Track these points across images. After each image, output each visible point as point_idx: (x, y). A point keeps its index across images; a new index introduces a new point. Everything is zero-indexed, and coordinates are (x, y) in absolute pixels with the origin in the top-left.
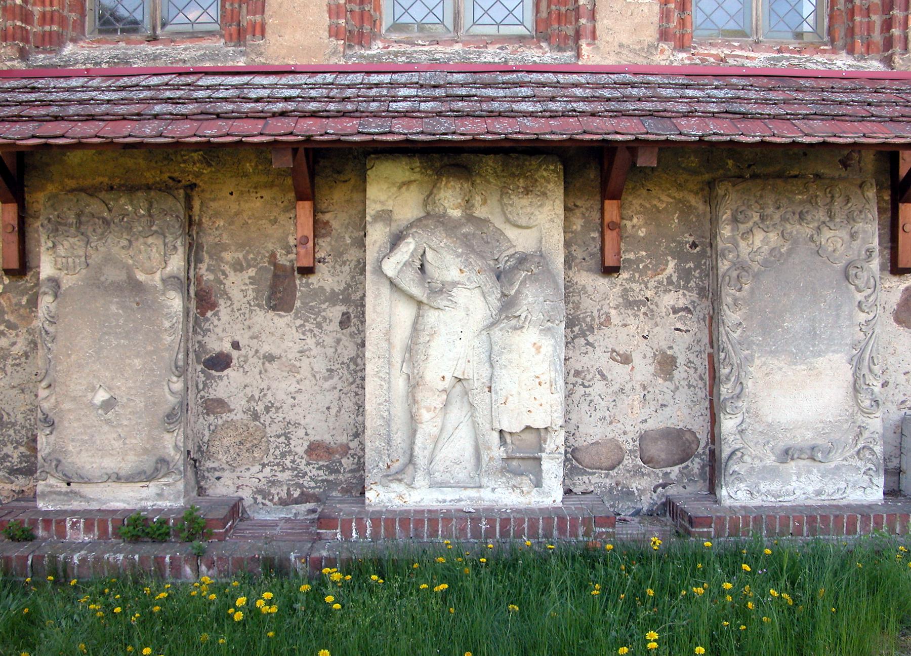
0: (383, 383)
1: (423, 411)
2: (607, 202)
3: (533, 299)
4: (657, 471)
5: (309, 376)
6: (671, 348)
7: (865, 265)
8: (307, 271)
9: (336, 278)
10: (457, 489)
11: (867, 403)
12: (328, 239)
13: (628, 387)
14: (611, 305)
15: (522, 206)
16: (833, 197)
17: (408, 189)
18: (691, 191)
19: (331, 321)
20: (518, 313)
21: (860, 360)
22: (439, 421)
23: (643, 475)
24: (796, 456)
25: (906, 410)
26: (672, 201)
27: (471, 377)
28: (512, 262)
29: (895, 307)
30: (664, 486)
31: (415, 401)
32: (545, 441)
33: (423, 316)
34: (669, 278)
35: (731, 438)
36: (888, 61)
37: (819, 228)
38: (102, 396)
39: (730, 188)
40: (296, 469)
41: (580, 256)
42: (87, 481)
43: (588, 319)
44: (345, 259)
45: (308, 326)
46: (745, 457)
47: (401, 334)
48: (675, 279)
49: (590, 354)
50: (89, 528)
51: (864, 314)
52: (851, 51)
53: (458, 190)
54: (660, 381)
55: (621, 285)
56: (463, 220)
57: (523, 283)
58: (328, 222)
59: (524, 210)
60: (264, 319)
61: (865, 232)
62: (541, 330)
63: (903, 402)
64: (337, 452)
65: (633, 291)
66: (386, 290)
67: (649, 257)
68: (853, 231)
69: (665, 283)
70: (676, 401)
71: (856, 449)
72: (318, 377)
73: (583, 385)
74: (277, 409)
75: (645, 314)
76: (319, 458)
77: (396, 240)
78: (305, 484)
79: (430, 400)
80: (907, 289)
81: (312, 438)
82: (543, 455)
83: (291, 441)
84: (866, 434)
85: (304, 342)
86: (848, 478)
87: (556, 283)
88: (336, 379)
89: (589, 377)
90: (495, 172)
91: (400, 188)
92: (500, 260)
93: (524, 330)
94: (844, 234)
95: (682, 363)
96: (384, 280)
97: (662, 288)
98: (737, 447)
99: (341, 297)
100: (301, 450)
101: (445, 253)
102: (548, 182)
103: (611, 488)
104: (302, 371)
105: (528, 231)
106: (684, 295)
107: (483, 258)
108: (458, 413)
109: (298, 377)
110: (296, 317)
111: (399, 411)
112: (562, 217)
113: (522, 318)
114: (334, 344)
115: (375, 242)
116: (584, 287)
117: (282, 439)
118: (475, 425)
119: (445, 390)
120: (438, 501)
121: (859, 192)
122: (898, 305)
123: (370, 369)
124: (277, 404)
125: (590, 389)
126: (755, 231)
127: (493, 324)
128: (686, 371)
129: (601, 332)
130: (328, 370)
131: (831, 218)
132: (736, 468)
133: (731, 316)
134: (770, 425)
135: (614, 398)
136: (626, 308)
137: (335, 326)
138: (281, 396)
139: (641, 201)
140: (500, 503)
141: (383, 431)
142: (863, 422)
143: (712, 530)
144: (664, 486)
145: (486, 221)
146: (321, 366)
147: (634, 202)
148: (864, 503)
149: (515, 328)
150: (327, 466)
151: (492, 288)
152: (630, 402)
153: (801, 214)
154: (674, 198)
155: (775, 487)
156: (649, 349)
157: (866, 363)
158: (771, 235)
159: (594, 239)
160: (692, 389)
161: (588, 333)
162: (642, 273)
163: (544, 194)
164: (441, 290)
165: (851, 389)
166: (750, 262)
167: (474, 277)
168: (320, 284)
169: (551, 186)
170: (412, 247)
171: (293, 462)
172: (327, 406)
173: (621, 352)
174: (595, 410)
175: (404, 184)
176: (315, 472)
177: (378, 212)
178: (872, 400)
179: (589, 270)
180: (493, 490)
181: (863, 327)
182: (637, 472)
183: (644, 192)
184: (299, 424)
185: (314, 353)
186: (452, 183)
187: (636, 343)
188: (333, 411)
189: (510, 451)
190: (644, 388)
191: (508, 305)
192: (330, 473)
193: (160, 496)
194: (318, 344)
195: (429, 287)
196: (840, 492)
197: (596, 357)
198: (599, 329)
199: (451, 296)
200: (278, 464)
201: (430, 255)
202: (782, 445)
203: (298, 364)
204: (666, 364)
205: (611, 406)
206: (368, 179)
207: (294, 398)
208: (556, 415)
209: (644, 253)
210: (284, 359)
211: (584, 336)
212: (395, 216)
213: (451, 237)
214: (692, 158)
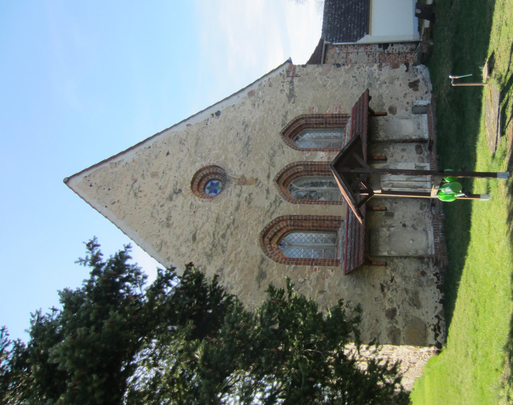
2: (376, 158)
36: (349, 117)
38: (411, 242)
42: (428, 244)
50: (436, 238)
52: (346, 124)
60: (395, 217)
133: (394, 138)
155: (425, 130)
182: (424, 155)
193: (430, 230)
204: (403, 150)
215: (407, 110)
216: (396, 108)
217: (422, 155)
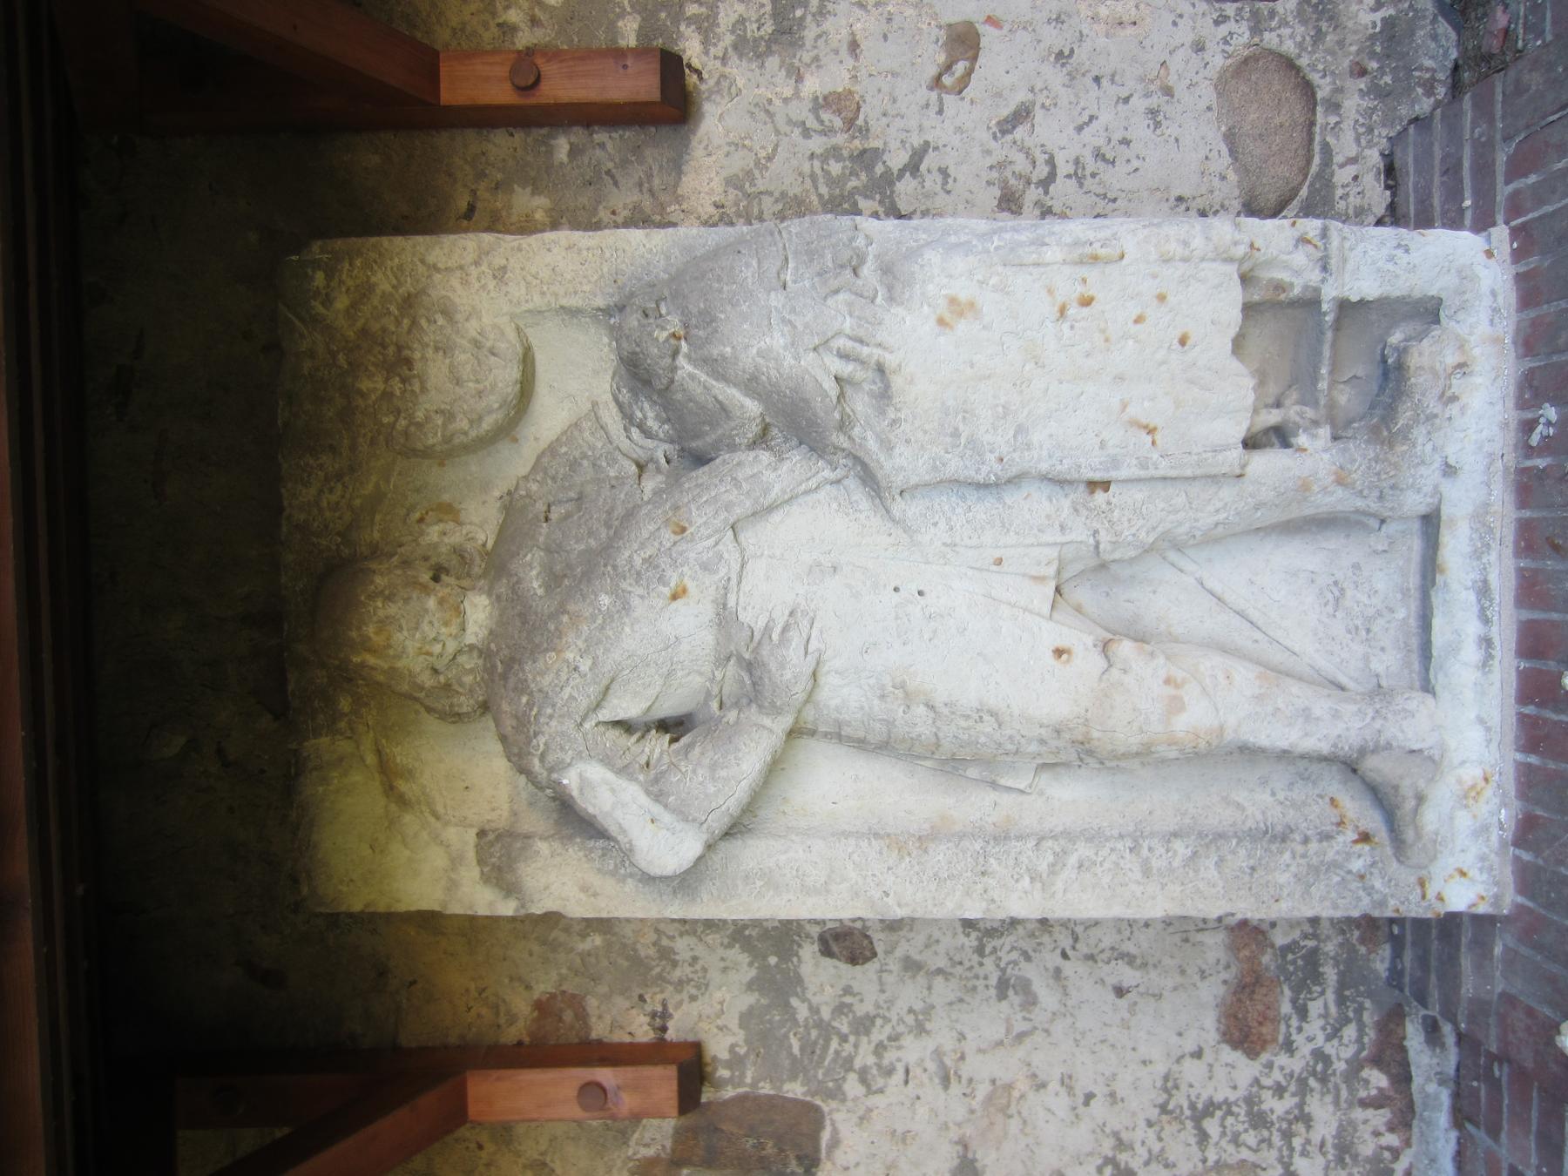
0: (1072, 860)
1: (1182, 724)
2: (447, 96)
3: (776, 330)
5: (1020, 1052)
8: (692, 1069)
9: (714, 975)
10: (1437, 599)
12: (592, 1003)
14: (788, 92)
15: (456, 379)
17: (409, 774)
19: (848, 991)
20: (830, 386)
22: (1211, 664)
27: (1053, 553)
28: (648, 413)
31: (1144, 754)
32: (1279, 287)
33: (839, 724)
40: (1303, 1083)
41: (633, 197)
43: (835, 168)
44: (652, 951)
45: (865, 1057)
47: (900, 794)
49: (949, 161)
53: (393, 609)
55: (724, 60)
56: (502, 588)
57: (717, 368)
58: (539, 1006)
59: (466, 372)
62: (891, 299)
64: (1252, 960)
65: (742, 21)
66: (752, 853)
72: (1025, 1026)
73: (1046, 183)
74: (1121, 1145)
76: (1269, 1017)
77: (572, 820)
78: (1348, 1053)
79: (1142, 701)
81: (1211, 1036)
82: (1330, 293)
83: (1219, 1098)
85: (916, 1071)
87: (715, 254)
88: (1029, 971)
89: (1021, 163)
90: (339, 476)
91: (403, 802)
92: (641, 455)
93: (890, 360)
96: (716, 859)
99: (773, 960)
100: (1245, 1069)
101: (616, 655)
102: (366, 290)
103: (1378, 92)
104: (1004, 1077)
105: (540, 358)
107: (630, 514)
108: (1169, 598)
109: (1022, 1085)
110: (837, 1094)
111: (1162, 802)
112: (487, 238)
113: (846, 369)
114: (921, 979)
115: (584, 889)
116: (732, 182)
117: (1212, 1126)
118: (1215, 538)
119: (1105, 647)
120: (1485, 664)
123: (1023, 903)
124: (1107, 1147)
127: (868, 477)
129: (875, 127)
130: (1002, 996)
135: (1088, 80)
136: (797, 43)
137: (863, 977)
138: (1081, 1137)
140: (1497, 447)
141: (1240, 859)
145: (512, 506)
146: (989, 1019)
147: (454, 21)
149: (884, 395)
150: (1297, 990)
151: (737, 484)
159: (574, 152)
161: (879, 169)
163: (409, 302)
164: (749, 666)
167: (699, 549)
168: (734, 1024)
169: (383, 282)
170: (596, 772)
171: (1279, 1091)
172: (1112, 996)
173: (942, 58)
174: (1126, 142)
175: (390, 789)
176: (1315, 1027)
177: (485, 879)
179: (677, 166)
180: (1449, 470)
184: (1166, 1078)
185: (946, 1040)
186: (370, 630)
188: (1128, 976)
189: (1310, 413)
191: (796, 424)
192: (1317, 977)
194: (920, 1030)
195: (737, 704)
197: (956, 140)
198: (865, 131)
199: (768, 629)
200: (1287, 1135)
201: (628, 706)
203: (983, 1090)
205: (1112, 91)
206: (381, 909)
207: (1089, 1097)
208: (1198, 242)
210: (968, 1131)
211: (889, 180)
212: (499, 816)
213: (560, 634)
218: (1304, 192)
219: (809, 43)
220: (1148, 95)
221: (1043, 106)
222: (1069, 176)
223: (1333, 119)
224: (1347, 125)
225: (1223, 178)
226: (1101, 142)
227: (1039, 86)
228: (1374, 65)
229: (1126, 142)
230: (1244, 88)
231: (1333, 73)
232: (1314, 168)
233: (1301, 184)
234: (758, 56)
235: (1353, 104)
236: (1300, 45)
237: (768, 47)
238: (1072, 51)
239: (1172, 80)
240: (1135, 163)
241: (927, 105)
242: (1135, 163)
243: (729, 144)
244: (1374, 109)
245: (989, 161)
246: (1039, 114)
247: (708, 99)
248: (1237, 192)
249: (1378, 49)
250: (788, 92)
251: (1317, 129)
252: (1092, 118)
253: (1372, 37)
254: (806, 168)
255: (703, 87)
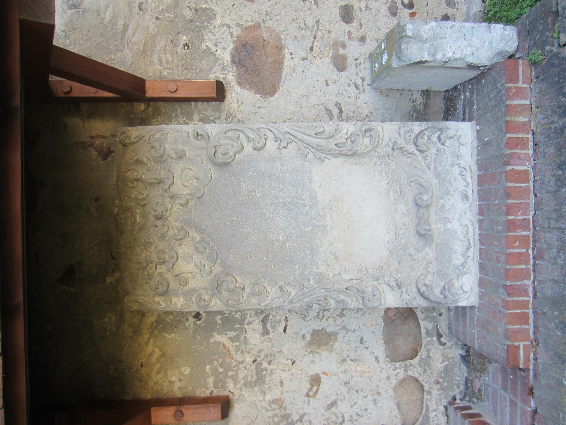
4: (424, 342)
6: (304, 336)
7: (213, 142)
11: (367, 141)
13: (343, 377)
14: (261, 399)
16: (137, 180)
18: (141, 320)
21: (319, 149)
23: (429, 357)
24: (428, 228)
25: (365, 83)
26: (152, 341)
29: (258, 96)
30: (440, 336)
34: (232, 339)
35: (406, 297)
37: (172, 197)
39: (132, 298)
43: (276, 419)
46: (428, 283)
48: (233, 334)
51: (268, 143)
54: (337, 345)
55: (241, 389)
61: (175, 141)
63: (357, 88)
65: (246, 376)
67: (211, 362)
68: (174, 156)
69: (238, 344)
70: (357, 328)
71: (418, 153)
75: (270, 363)
80: (240, 84)
84: (401, 142)
86: (449, 163)
89: (334, 418)
94: (177, 167)
95: (319, 324)
97: (243, 347)
98: (415, 290)
103: (442, 388)
106: (249, 323)
121: (131, 147)
122: (257, 93)
125: (346, 416)
126: (176, 272)
128: (327, 320)
131: (160, 182)
132: (437, 291)
134: (391, 253)
135: (354, 391)
136: (264, 382)
139: (154, 373)
142: (387, 145)
143: (521, 344)
144: (440, 336)
147: (155, 380)
148: (475, 144)
152: (358, 374)
153: (158, 218)
154: (149, 339)
155: (458, 247)
156: (305, 359)
157: (322, 142)
158: (180, 252)
160: (345, 312)
161: (290, 420)
162: (228, 368)
165: (352, 160)
166: (212, 276)
174: (366, 410)
178: (364, 136)
181: (283, 144)
182: (426, 363)
183: (144, 370)
187: (299, 372)
190: (344, 360)
196: (464, 173)
198: (285, 408)
202: (414, 239)
209: (208, 367)
214: (106, 320)
215: (340, 64)
216: (280, 48)
217: (415, 368)
218: (420, 420)
219: (267, 382)
220: (373, 395)
221: (340, 400)
222: (348, 421)
223: (429, 397)
224: (433, 399)
225: (396, 417)
226: (358, 410)
227: (339, 393)
228: (442, 380)
229: (366, 410)
230: (402, 389)
231: (429, 382)
232: (424, 412)
233: (419, 418)
234: (252, 387)
235: (435, 392)
236: (419, 374)
237: (255, 384)
238: (349, 382)
239: (380, 390)
240: (369, 416)
241: (305, 402)
242: (369, 416)
243: (243, 417)
244: (441, 394)
245: (324, 418)
246: (339, 402)
247: (236, 402)
248: (400, 421)
249: (443, 375)
250: (261, 399)
251: (424, 400)
252: (356, 403)
253: (441, 372)
254: (267, 420)
255: (234, 398)
